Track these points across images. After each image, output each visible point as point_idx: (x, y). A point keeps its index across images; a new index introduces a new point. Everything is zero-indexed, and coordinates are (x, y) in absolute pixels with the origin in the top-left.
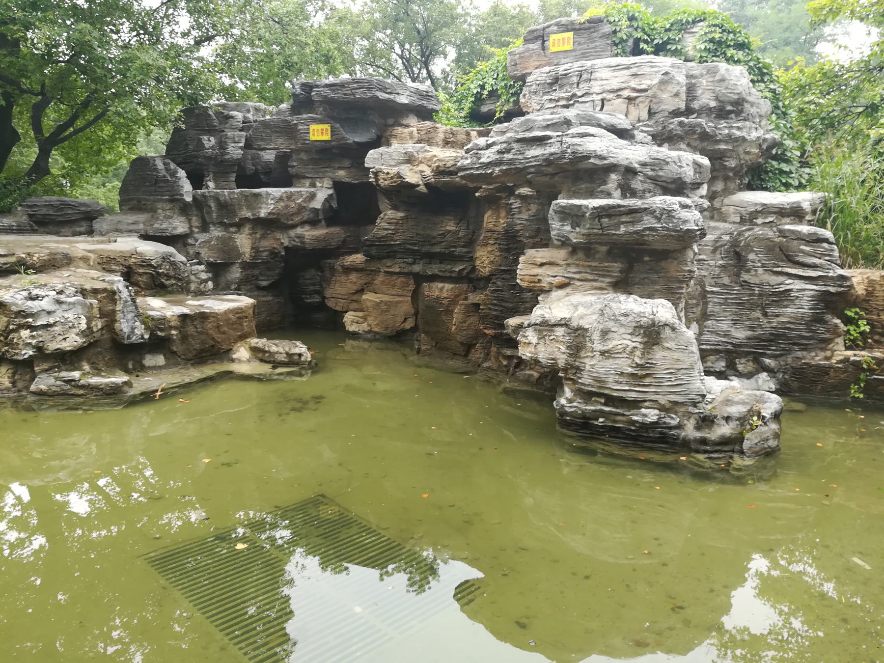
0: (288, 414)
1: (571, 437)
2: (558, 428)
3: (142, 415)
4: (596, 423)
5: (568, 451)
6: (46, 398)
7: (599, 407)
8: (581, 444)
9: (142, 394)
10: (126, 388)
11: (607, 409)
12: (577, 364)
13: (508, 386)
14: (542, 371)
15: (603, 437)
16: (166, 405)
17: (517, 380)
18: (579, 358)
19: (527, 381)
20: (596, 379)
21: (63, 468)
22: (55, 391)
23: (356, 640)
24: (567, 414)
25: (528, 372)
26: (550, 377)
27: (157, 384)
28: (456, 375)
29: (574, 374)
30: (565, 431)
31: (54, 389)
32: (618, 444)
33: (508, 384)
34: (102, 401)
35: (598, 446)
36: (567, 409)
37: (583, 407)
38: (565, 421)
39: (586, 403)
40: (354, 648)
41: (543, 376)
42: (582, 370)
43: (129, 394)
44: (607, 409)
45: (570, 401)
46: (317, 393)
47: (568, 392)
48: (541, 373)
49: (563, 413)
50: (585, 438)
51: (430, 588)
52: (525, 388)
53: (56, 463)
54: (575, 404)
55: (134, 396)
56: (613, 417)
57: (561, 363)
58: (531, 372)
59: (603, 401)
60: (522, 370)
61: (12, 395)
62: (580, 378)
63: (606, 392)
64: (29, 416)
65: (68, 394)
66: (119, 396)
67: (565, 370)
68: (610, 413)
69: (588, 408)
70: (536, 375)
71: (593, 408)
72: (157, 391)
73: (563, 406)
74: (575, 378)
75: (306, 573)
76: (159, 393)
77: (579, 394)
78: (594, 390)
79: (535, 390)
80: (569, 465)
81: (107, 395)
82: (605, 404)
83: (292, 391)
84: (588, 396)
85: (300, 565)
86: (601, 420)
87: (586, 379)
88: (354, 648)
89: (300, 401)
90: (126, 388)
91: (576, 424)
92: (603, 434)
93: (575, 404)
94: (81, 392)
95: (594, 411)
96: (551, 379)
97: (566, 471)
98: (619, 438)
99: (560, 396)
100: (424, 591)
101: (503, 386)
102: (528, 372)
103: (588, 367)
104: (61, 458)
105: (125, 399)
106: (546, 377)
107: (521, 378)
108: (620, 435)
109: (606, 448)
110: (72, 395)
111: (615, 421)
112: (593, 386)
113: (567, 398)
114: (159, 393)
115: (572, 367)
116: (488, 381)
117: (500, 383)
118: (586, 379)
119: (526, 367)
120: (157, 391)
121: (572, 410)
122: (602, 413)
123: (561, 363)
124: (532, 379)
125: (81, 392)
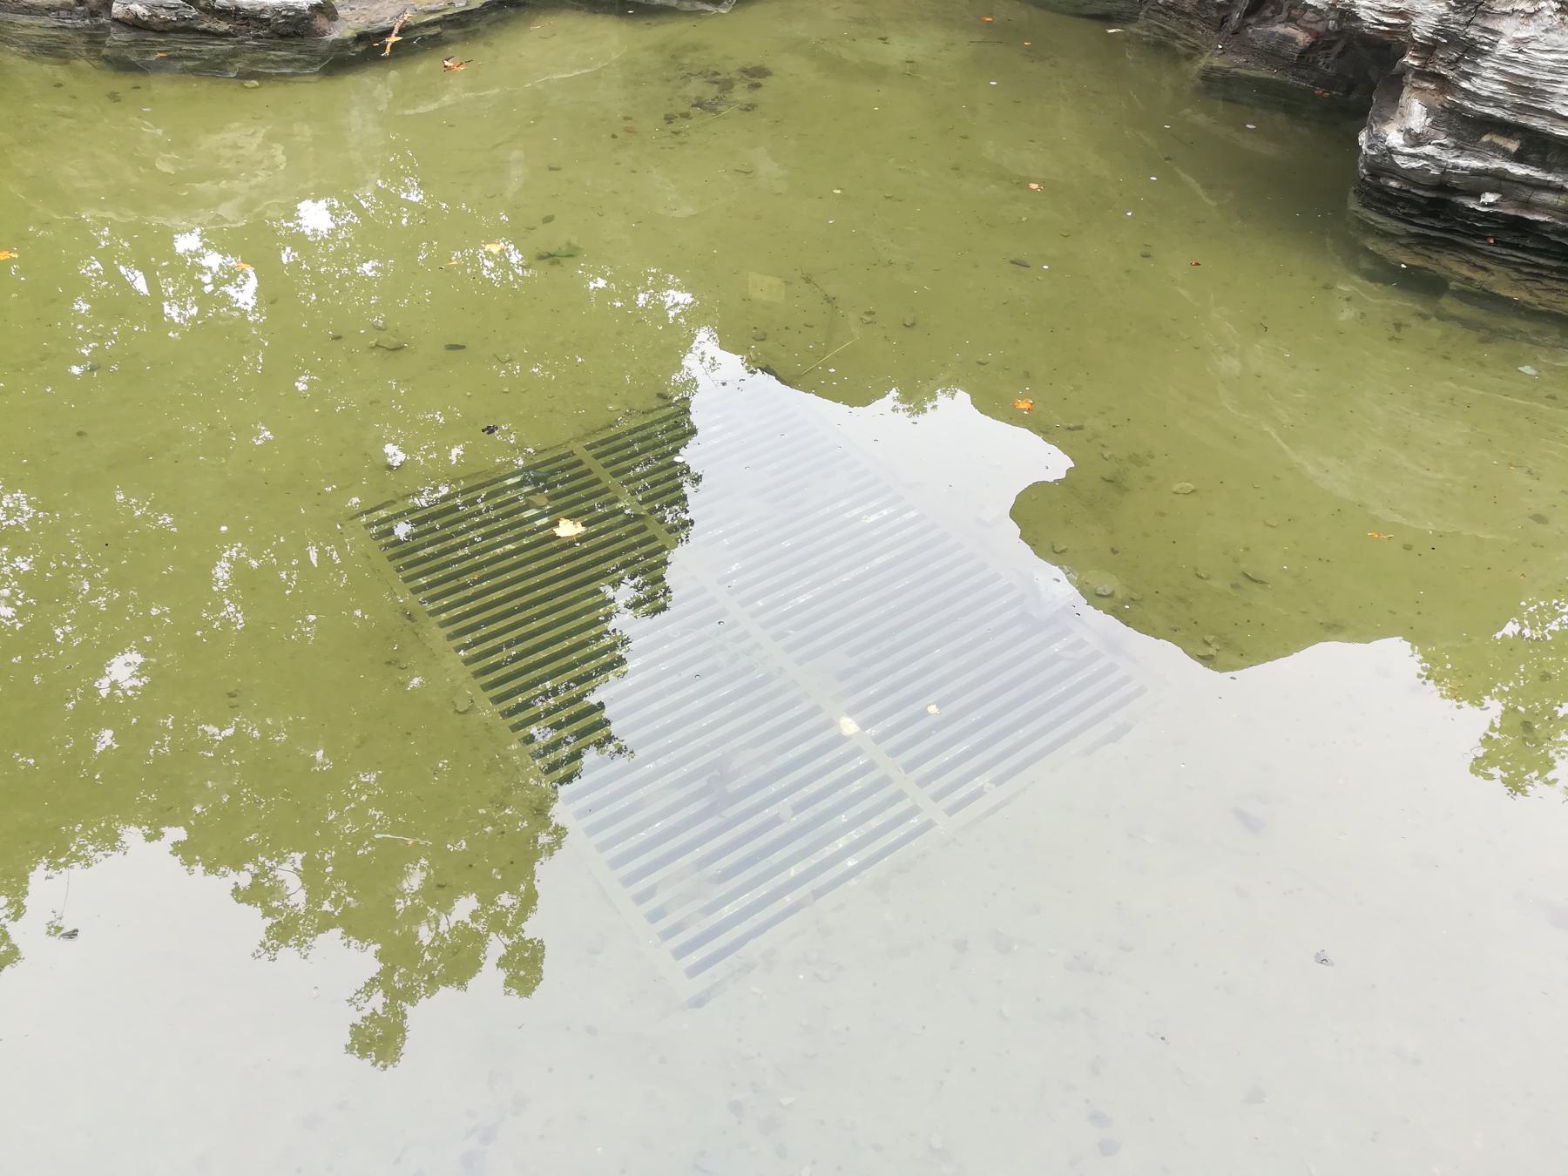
0: (686, 116)
1: (1386, 236)
2: (1354, 205)
3: (371, 91)
4: (1472, 204)
5: (1371, 276)
6: (152, 38)
7: (1496, 164)
8: (1405, 260)
9: (361, 37)
10: (321, 22)
11: (1518, 170)
12: (1473, 32)
13: (1216, 62)
14: (1319, 27)
15: (1477, 244)
16: (422, 67)
17: (1245, 47)
18: (1485, 14)
19: (1274, 53)
20: (1521, 87)
21: (225, 196)
22: (167, 22)
23: (843, 818)
24: (1394, 172)
25: (1280, 29)
26: (1338, 48)
27: (392, 12)
28: (1082, 21)
29: (1453, 64)
30: (1373, 217)
31: (163, 14)
32: (1516, 267)
33: (1215, 58)
34: (273, 55)
35: (1455, 267)
36: (1399, 160)
37: (1449, 158)
38: (1383, 190)
39: (1460, 149)
40: (841, 843)
41: (1321, 42)
42: (1482, 53)
43: (329, 38)
44: (1518, 170)
45: (1415, 139)
46: (754, 59)
47: (1415, 113)
48: (1318, 36)
49: (1383, 165)
50: (1425, 241)
51: (934, 407)
52: (1263, 73)
53: (205, 186)
54: (1428, 149)
55: (342, 44)
56: (1525, 193)
57: (1423, 28)
58: (1290, 30)
59: (1513, 146)
60: (1265, 20)
61: (79, 23)
62: (1467, 76)
63: (1536, 123)
64: (122, 83)
65: (196, 31)
66: (308, 43)
67: (1428, 49)
68: (1526, 182)
69: (1462, 162)
70: (1302, 38)
71: (1476, 164)
72: (388, 32)
73: (1391, 151)
74: (1451, 74)
75: (719, 375)
76: (393, 39)
77: (1448, 123)
78: (1498, 113)
79: (1290, 79)
80: (1354, 304)
81: (282, 36)
82: (1518, 158)
83: (695, 48)
84: (1468, 126)
85: (707, 358)
86: (1489, 198)
87: (1485, 82)
88: (841, 843)
89: (712, 77)
90: (321, 22)
91: (1411, 202)
92: (1480, 235)
93: (1428, 149)
94: (223, 26)
95: (1476, 172)
96: (1341, 54)
97: (1347, 314)
98: (1525, 249)
99: (1386, 120)
100: (924, 411)
101: (1202, 62)
102: (1280, 29)
103: (1504, 47)
104: (216, 176)
105: (322, 48)
106: (1329, 45)
107: (1259, 43)
108: (1529, 243)
109: (1479, 276)
110: (205, 32)
111: (1528, 205)
112: (1498, 104)
113: (1408, 131)
114: (393, 39)
115: (1454, 40)
116: (1160, 47)
117: (1194, 52)
118: (1485, 83)
119: (1278, 12)
120: (388, 32)
121: (1414, 164)
122: (1499, 181)
123: (1423, 28)
124: (1288, 50)
125: (223, 26)
